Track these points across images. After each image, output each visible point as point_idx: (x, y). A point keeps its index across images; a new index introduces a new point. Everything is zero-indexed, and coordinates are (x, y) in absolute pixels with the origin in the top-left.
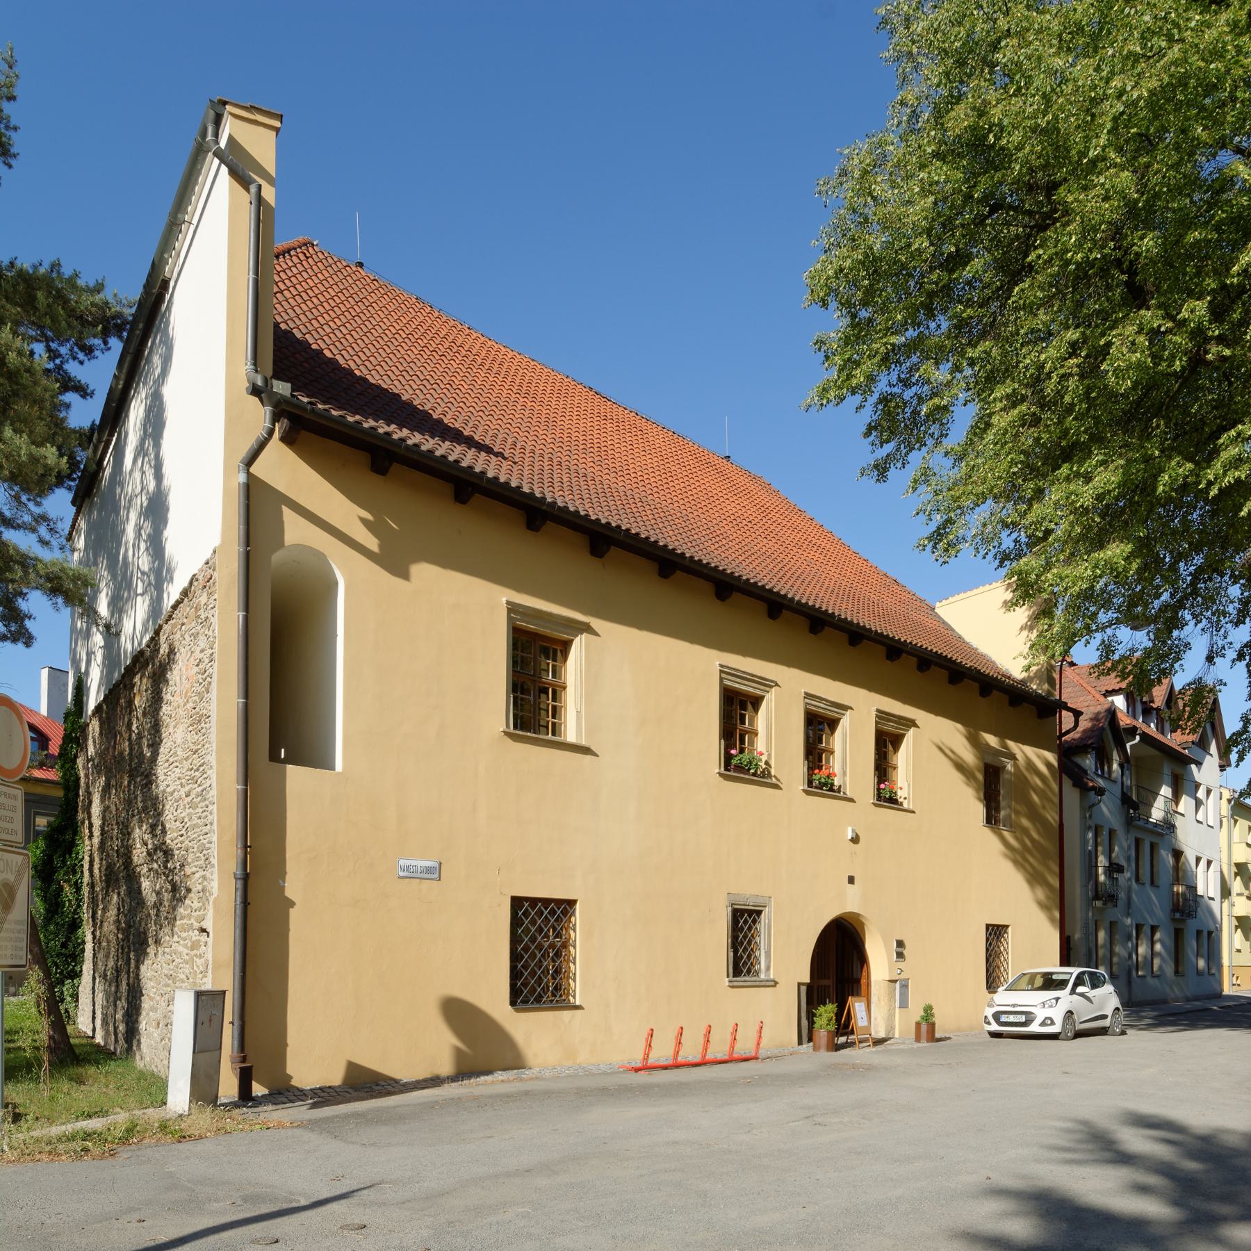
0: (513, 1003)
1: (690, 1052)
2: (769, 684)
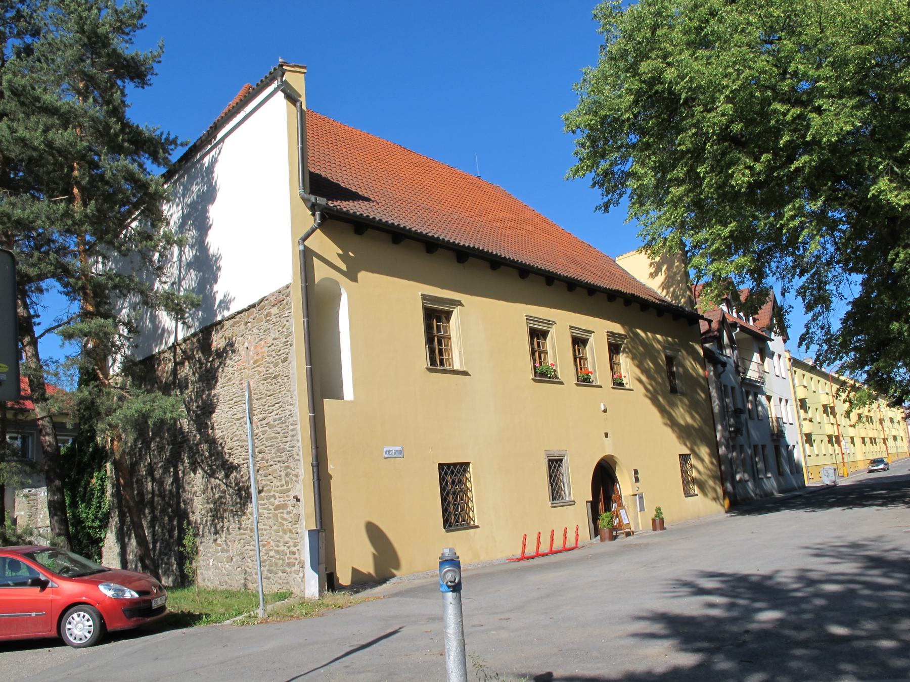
0: (445, 527)
1: (545, 548)
2: (551, 323)
